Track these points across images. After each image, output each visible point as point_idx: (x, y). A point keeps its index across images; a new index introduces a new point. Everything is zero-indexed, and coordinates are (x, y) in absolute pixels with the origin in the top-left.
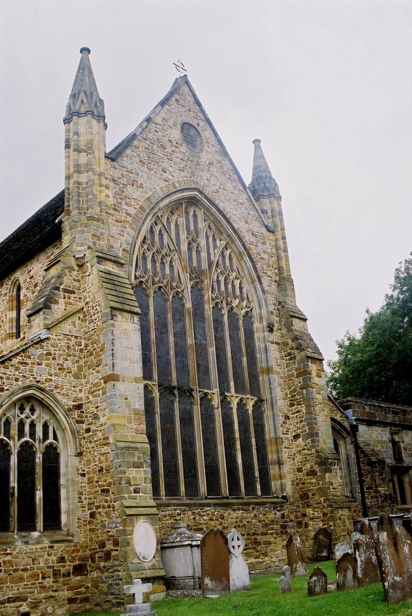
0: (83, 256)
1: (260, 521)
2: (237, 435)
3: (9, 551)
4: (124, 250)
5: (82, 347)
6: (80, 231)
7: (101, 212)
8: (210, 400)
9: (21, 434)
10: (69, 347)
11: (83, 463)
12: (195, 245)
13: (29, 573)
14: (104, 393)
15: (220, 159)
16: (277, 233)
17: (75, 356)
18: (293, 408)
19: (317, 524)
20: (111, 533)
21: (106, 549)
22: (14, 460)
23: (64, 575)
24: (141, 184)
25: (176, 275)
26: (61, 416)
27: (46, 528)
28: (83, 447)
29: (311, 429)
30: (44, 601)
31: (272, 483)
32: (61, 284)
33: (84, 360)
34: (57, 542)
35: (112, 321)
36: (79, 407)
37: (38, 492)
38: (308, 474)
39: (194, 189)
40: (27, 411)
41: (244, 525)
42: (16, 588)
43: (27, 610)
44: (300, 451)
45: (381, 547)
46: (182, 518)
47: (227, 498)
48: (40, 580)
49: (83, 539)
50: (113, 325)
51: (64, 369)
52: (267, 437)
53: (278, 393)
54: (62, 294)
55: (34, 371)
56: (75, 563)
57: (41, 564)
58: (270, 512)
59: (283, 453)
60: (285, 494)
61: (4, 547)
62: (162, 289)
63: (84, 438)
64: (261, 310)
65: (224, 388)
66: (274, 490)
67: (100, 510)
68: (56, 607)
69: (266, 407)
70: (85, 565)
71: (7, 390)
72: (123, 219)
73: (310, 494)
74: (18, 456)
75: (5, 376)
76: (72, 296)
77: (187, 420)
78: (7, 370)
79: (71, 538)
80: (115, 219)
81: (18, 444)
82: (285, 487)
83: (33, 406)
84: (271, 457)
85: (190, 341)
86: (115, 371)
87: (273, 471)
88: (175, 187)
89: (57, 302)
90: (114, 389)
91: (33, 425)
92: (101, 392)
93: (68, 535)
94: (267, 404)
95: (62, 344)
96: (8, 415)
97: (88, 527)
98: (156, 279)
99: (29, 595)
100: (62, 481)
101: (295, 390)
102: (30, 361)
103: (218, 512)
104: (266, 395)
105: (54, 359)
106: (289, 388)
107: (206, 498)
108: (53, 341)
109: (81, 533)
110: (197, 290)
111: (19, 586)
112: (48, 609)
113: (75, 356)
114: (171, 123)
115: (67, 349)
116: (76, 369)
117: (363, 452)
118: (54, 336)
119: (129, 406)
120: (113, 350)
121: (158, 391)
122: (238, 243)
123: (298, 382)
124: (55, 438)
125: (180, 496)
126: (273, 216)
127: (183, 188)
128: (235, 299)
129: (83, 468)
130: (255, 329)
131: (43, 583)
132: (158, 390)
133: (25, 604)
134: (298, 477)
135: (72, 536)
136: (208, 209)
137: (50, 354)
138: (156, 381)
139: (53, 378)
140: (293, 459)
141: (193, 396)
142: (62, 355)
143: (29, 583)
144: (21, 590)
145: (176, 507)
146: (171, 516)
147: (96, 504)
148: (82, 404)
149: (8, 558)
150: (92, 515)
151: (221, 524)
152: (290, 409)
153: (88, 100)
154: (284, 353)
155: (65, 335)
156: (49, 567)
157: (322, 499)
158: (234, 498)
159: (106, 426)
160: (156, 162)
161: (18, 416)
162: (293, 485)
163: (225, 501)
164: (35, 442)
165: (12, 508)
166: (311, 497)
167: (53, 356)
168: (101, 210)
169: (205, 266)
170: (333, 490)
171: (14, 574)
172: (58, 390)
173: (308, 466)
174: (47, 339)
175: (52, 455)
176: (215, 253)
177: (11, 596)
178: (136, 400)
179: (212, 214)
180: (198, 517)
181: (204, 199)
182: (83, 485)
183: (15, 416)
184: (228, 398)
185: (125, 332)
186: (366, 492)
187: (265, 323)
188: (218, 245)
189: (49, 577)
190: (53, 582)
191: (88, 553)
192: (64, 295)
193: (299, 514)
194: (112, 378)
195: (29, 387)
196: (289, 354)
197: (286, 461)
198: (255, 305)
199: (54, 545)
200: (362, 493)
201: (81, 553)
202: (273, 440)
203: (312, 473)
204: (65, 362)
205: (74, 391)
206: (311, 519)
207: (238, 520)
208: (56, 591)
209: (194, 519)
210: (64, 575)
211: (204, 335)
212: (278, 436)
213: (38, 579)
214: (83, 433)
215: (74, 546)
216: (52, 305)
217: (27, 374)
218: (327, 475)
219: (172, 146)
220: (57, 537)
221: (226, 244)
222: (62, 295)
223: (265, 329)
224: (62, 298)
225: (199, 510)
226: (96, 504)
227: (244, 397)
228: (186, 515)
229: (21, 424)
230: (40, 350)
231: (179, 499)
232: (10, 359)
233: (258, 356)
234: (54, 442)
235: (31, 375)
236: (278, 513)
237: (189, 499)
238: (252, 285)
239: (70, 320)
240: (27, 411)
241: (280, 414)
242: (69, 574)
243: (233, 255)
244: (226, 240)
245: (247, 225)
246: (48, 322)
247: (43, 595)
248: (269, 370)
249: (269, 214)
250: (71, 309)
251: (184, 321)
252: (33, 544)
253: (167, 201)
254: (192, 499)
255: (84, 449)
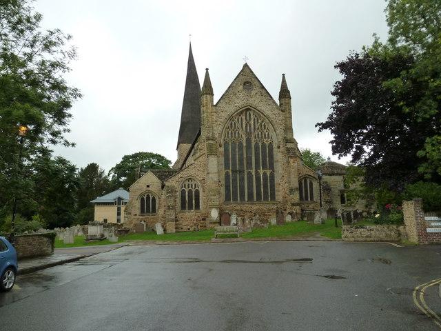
22: (187, 193)
65: (257, 167)
77: (242, 180)
91: (192, 185)
110: (249, 141)
175: (197, 193)
229: (189, 185)
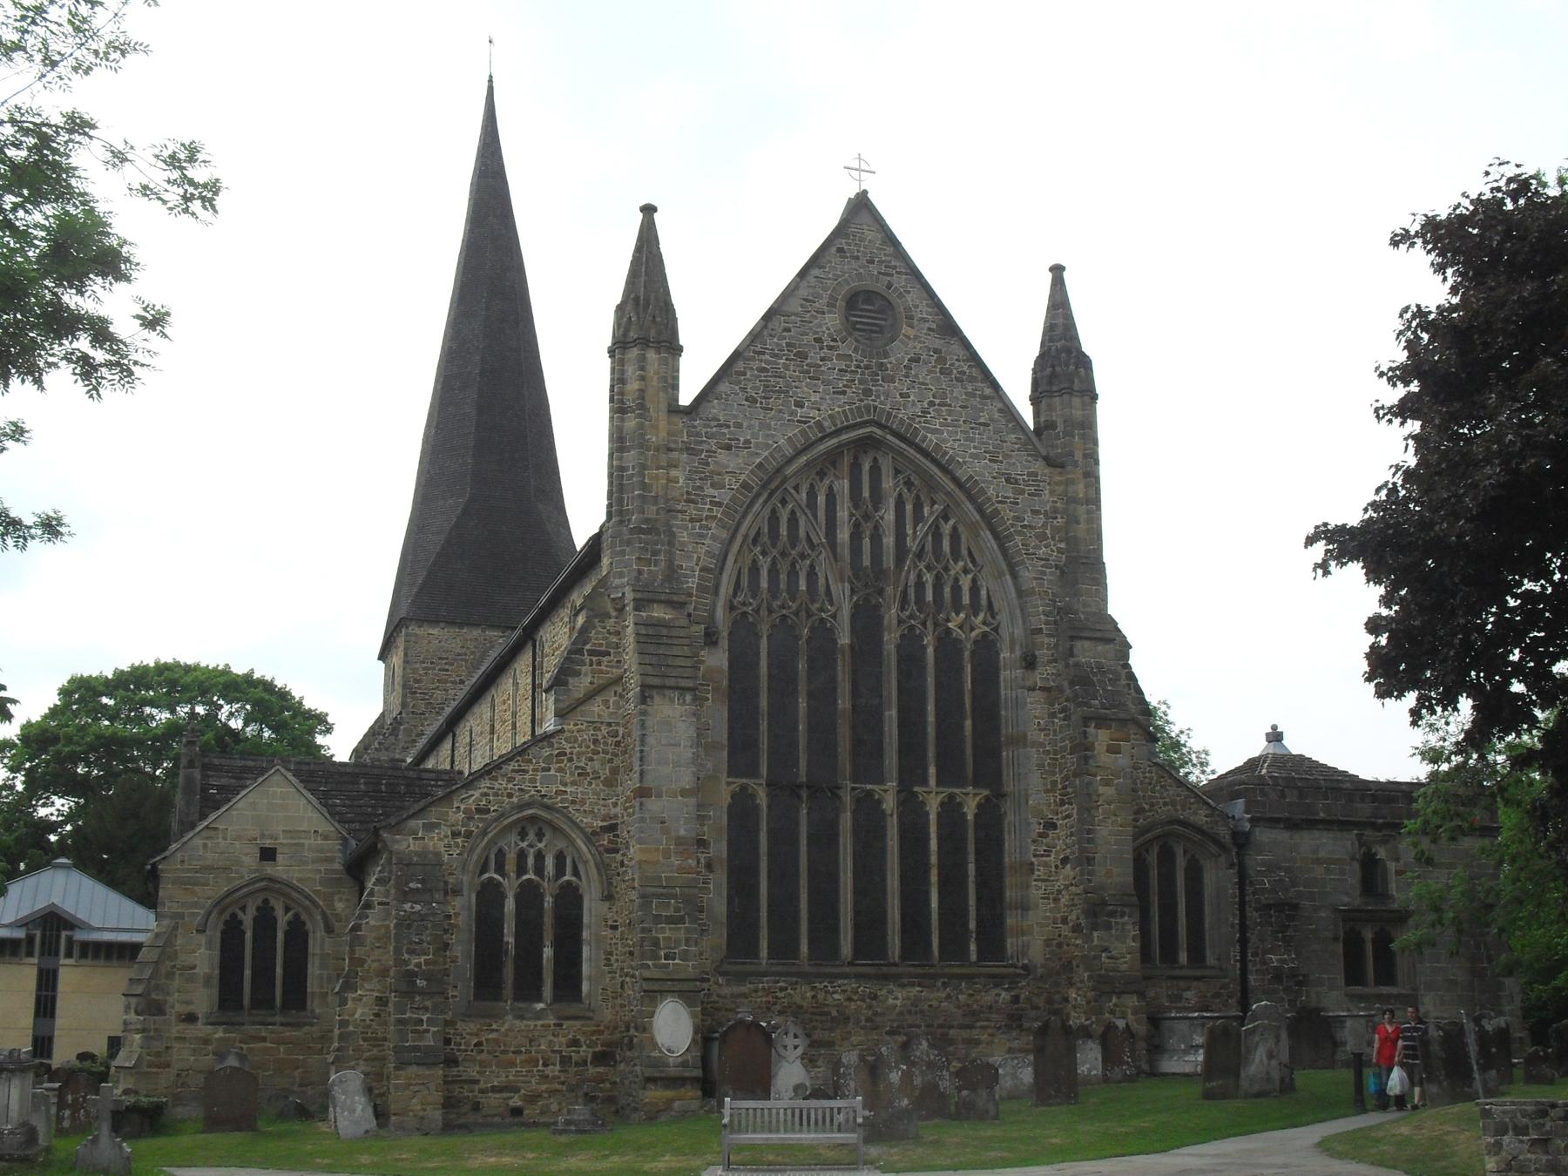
0: (620, 595)
2: (934, 859)
3: (494, 1027)
4: (703, 569)
5: (618, 739)
8: (880, 802)
9: (521, 869)
12: (867, 529)
13: (523, 1057)
15: (938, 343)
22: (510, 905)
23: (577, 1064)
27: (557, 998)
30: (546, 1095)
31: (1009, 941)
32: (585, 644)
36: (612, 828)
37: (970, 865)
40: (531, 836)
43: (520, 1103)
44: (1067, 887)
46: (790, 994)
47: (895, 965)
48: (540, 1068)
49: (609, 1018)
52: (1007, 860)
53: (1035, 781)
54: (587, 658)
56: (597, 1050)
61: (488, 1021)
65: (911, 775)
66: (1009, 951)
69: (1008, 807)
75: (490, 792)
76: (605, 659)
77: (825, 838)
79: (591, 1014)
83: (540, 829)
85: (844, 703)
91: (540, 857)
98: (776, 604)
100: (585, 934)
104: (1009, 787)
105: (571, 760)
107: (851, 964)
108: (569, 734)
114: (821, 303)
116: (607, 771)
118: (571, 727)
119: (666, 831)
122: (969, 506)
124: (576, 873)
125: (798, 959)
129: (616, 918)
135: (593, 1011)
136: (901, 453)
141: (839, 798)
142: (583, 753)
144: (511, 1078)
146: (767, 992)
151: (870, 1007)
153: (639, 318)
156: (553, 1051)
157: (1086, 975)
158: (913, 965)
162: (1047, 945)
163: (894, 970)
170: (1107, 961)
172: (577, 807)
174: (561, 731)
175: (570, 899)
177: (496, 1084)
178: (682, 822)
179: (911, 461)
180: (821, 996)
182: (614, 941)
183: (512, 844)
189: (554, 1065)
192: (591, 660)
195: (529, 805)
200: (1243, 961)
201: (606, 1036)
207: (908, 1002)
210: (577, 1064)
213: (537, 1066)
215: (594, 1026)
219: (821, 348)
220: (573, 1009)
222: (587, 661)
227: (957, 791)
228: (798, 991)
229: (522, 855)
232: (498, 767)
233: (1003, 713)
234: (574, 879)
236: (1003, 994)
237: (816, 965)
239: (599, 699)
240: (531, 836)
241: (1034, 820)
243: (961, 529)
245: (995, 466)
247: (544, 1087)
250: (598, 681)
251: (835, 669)
252: (530, 1019)
254: (821, 965)
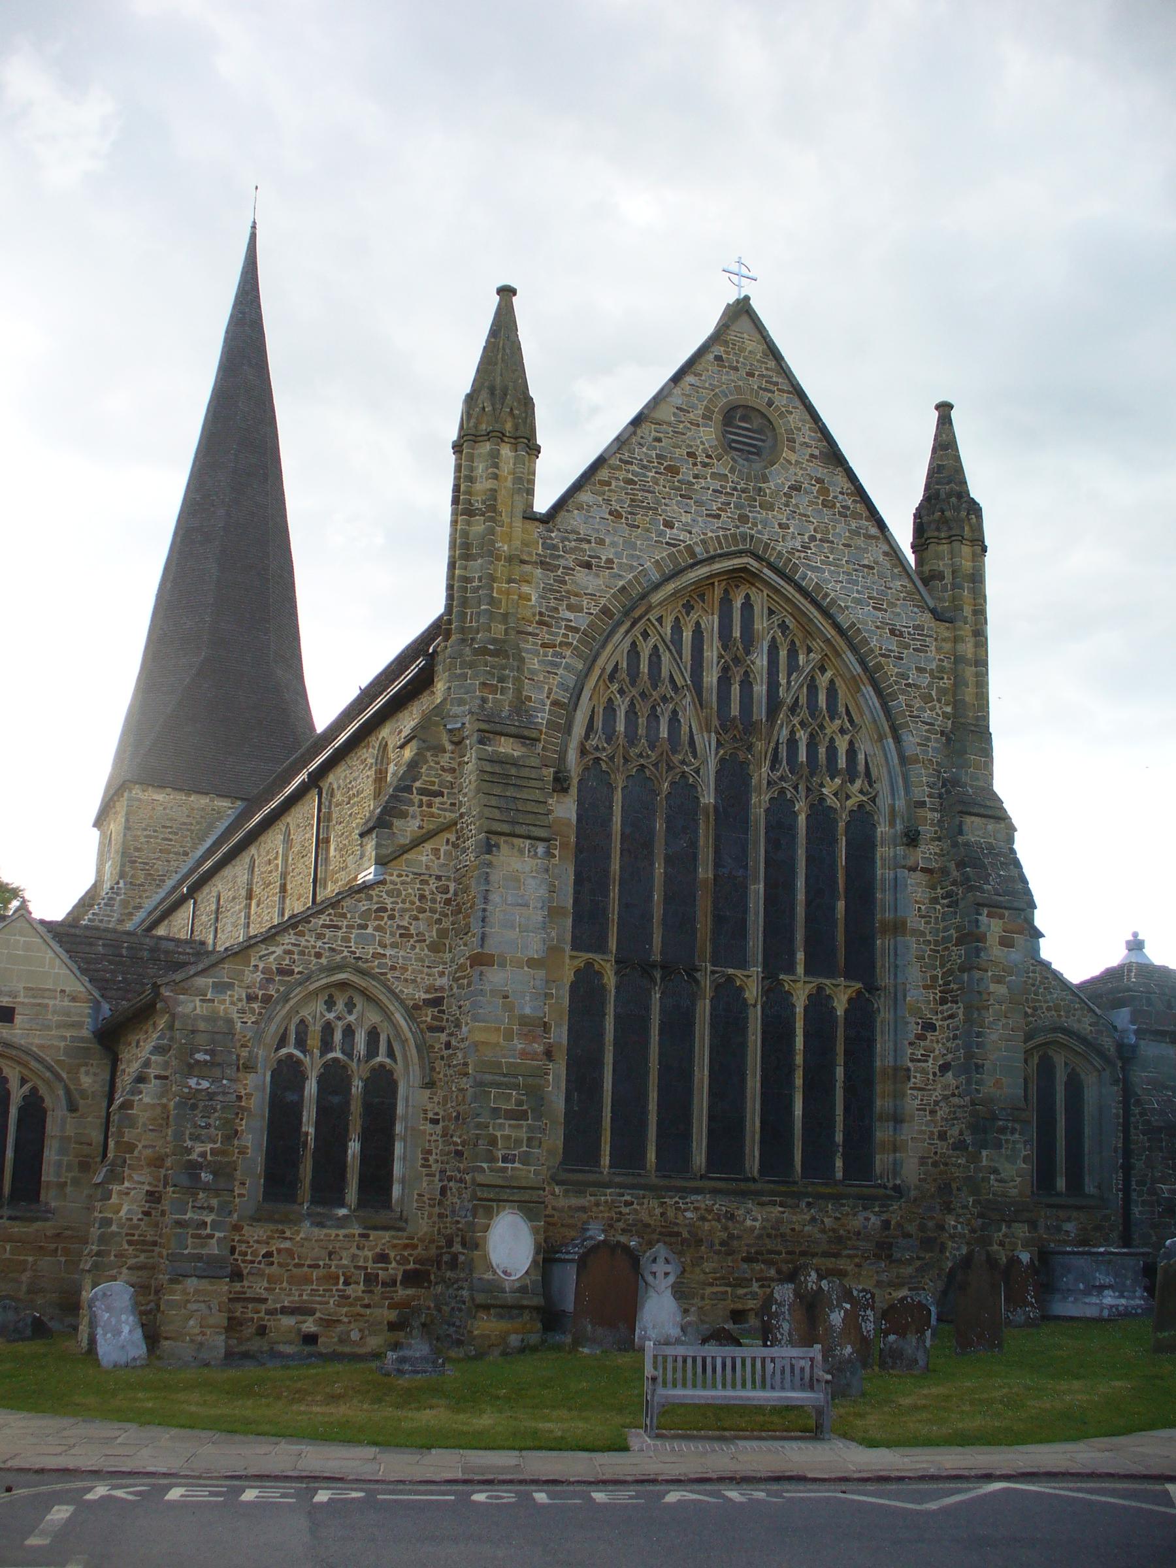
0: (459, 725)
1: (823, 1231)
3: (288, 1234)
4: (555, 703)
5: (448, 896)
6: (461, 674)
7: (505, 635)
8: (741, 989)
9: (327, 1046)
10: (422, 897)
11: (436, 1100)
13: (321, 1272)
14: (469, 985)
15: (821, 472)
16: (960, 624)
17: (433, 911)
18: (945, 1007)
19: (958, 1249)
20: (460, 1226)
21: (453, 1249)
23: (384, 1284)
24: (609, 561)
25: (685, 738)
26: (399, 1018)
27: (361, 1204)
28: (439, 1073)
29: (969, 1056)
30: (346, 1320)
31: (878, 1157)
33: (451, 919)
34: (375, 1228)
35: (487, 856)
36: (436, 1002)
37: (351, 1144)
38: (955, 1147)
39: (739, 554)
40: (340, 1006)
41: (782, 1235)
42: (297, 1294)
44: (945, 1098)
45: (774, 1307)
47: (754, 1180)
48: (341, 1287)
49: (425, 1229)
50: (490, 864)
51: (411, 936)
52: (878, 1063)
53: (914, 976)
54: (416, 798)
55: (352, 941)
56: (408, 1267)
57: (344, 1262)
58: (855, 1215)
59: (908, 1099)
60: (898, 1182)
62: (646, 770)
63: (442, 1058)
64: (893, 799)
66: (878, 1171)
67: (452, 1184)
68: (367, 1332)
70: (428, 1273)
71: (299, 973)
72: (559, 639)
73: (954, 1186)
74: (318, 1082)
75: (295, 949)
76: (438, 800)
78: (301, 939)
79: (404, 1225)
80: (540, 642)
81: (319, 1063)
82: (901, 1167)
84: (881, 1104)
85: (705, 872)
86: (486, 945)
87: (882, 1133)
88: (693, 554)
89: (404, 815)
90: (481, 980)
91: (349, 1032)
92: (465, 981)
93: (401, 1218)
94: (885, 997)
95: (410, 891)
96: (305, 1013)
97: (437, 1210)
99: (318, 1306)
100: (399, 1128)
101: (950, 972)
102: (345, 923)
103: (720, 1205)
104: (885, 979)
105: (391, 917)
106: (942, 966)
108: (392, 887)
109: (423, 1218)
111: (304, 1290)
112: (352, 1333)
113: (433, 911)
115: (419, 900)
117: (1138, 1102)
118: (394, 878)
120: (484, 910)
121: (616, 974)
122: (850, 657)
123: (958, 954)
124: (391, 1054)
126: (955, 586)
127: (712, 553)
128: (832, 779)
129: (437, 1110)
130: (879, 839)
131: (345, 1291)
132: (613, 972)
133: (311, 1319)
134: (939, 1151)
137: (385, 910)
138: (611, 952)
139: (388, 952)
140: (933, 1112)
141: (697, 982)
143: (321, 1288)
145: (622, 1190)
147: (448, 1173)
148: (443, 998)
149: (287, 1245)
150: (443, 1191)
152: (941, 1008)
154: (941, 891)
155: (416, 874)
157: (971, 1199)
159: (467, 1043)
160: (650, 508)
161: (323, 1016)
163: (752, 1186)
164: (353, 1060)
165: (302, 1166)
166: (955, 1192)
167: (389, 913)
168: (506, 630)
169: (760, 712)
171: (295, 1270)
172: (397, 974)
173: (954, 1132)
176: (789, 682)
177: (286, 1304)
180: (671, 1213)
181: (766, 571)
182: (434, 1137)
184: (786, 985)
185: (515, 879)
186: (1135, 1190)
187: (899, 827)
188: (801, 663)
189: (358, 1283)
190: (363, 1292)
191: (433, 1251)
192: (421, 800)
193: (930, 1224)
194: (481, 960)
195: (340, 968)
196: (948, 895)
197: (912, 1116)
198: (883, 787)
199: (370, 1232)
200: (1126, 1190)
202: (890, 1071)
203: (960, 1146)
204: (414, 923)
205: (429, 975)
206: (952, 1237)
208: (368, 1306)
209: (662, 1214)
210: (384, 1284)
211: (742, 860)
212: (899, 1063)
214: (440, 1049)
216: (395, 820)
217: (337, 945)
218: (984, 1153)
219: (695, 464)
221: (822, 659)
223: (899, 841)
224: (416, 804)
225: (677, 1199)
226: (448, 1173)
227: (827, 982)
229: (328, 1029)
230: (365, 903)
231: (639, 1175)
233: (879, 896)
234: (388, 1060)
235: (346, 947)
237: (664, 1176)
238: (879, 744)
239: (428, 846)
240: (340, 1006)
241: (912, 1020)
242: (394, 1283)
243: (839, 683)
244: (823, 650)
246: (384, 851)
248: (898, 927)
249: (945, 581)
251: (696, 831)
253: (670, 587)
254: (670, 1177)
255: (441, 1076)
